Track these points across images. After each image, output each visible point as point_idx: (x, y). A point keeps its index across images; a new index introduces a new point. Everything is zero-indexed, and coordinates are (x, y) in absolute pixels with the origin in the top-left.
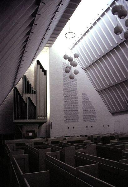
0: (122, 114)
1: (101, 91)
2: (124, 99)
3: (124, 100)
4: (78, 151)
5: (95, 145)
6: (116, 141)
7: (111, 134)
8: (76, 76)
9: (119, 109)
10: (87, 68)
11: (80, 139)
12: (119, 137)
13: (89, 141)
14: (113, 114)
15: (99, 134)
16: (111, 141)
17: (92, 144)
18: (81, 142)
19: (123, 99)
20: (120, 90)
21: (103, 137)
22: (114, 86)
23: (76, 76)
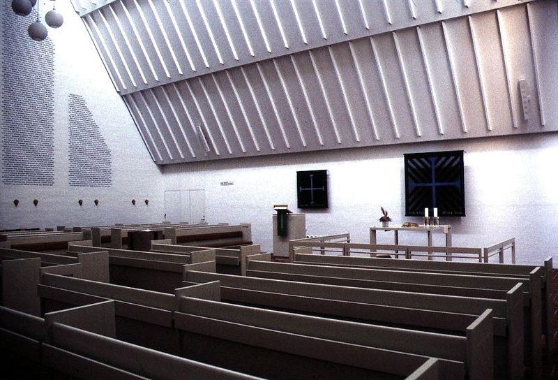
0: (379, 158)
1: (132, 94)
2: (197, 128)
3: (198, 131)
4: (48, 271)
5: (105, 252)
6: (166, 243)
7: (153, 226)
8: (51, 32)
9: (272, 145)
10: (92, 14)
11: (60, 237)
12: (178, 234)
13: (88, 244)
14: (164, 168)
15: (117, 225)
16: (154, 242)
17: (97, 250)
18: (62, 246)
19: (194, 128)
20: (163, 103)
21: (130, 234)
22: (171, 84)
23: (51, 32)
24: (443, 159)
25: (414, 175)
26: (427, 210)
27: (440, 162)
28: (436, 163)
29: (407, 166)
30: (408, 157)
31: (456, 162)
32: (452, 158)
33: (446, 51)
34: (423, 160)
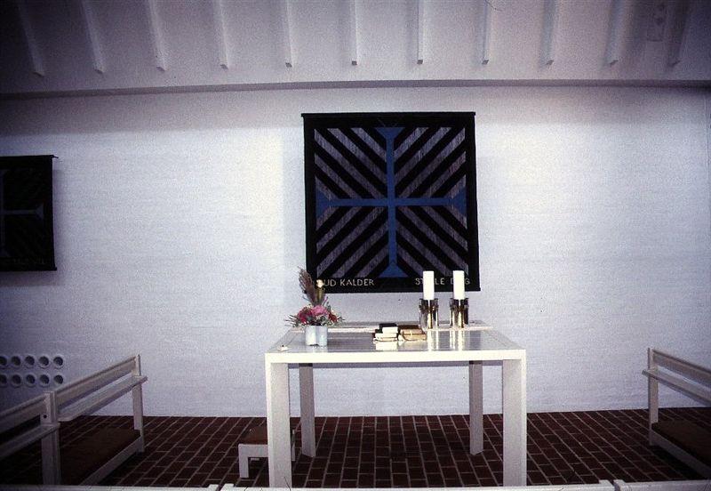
24: (418, 133)
25: (419, 155)
26: (428, 278)
27: (409, 141)
28: (398, 141)
29: (311, 148)
30: (314, 123)
31: (454, 144)
32: (442, 132)
33: (671, 439)
34: (360, 132)
